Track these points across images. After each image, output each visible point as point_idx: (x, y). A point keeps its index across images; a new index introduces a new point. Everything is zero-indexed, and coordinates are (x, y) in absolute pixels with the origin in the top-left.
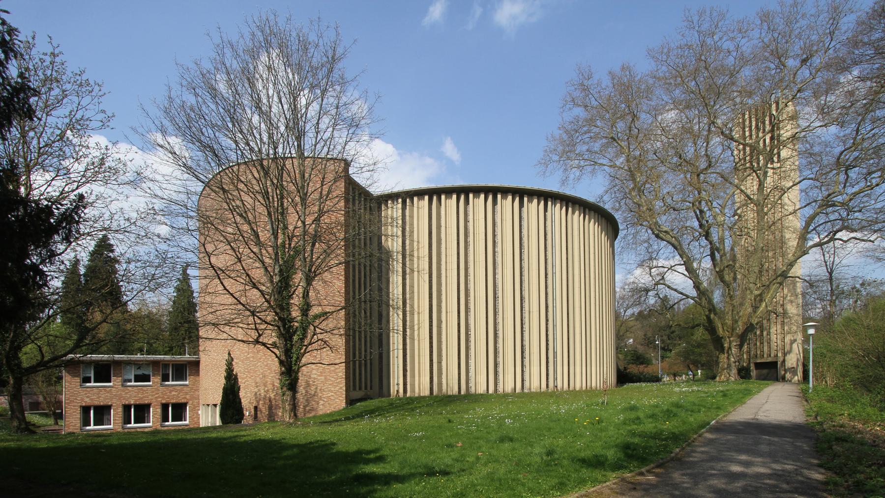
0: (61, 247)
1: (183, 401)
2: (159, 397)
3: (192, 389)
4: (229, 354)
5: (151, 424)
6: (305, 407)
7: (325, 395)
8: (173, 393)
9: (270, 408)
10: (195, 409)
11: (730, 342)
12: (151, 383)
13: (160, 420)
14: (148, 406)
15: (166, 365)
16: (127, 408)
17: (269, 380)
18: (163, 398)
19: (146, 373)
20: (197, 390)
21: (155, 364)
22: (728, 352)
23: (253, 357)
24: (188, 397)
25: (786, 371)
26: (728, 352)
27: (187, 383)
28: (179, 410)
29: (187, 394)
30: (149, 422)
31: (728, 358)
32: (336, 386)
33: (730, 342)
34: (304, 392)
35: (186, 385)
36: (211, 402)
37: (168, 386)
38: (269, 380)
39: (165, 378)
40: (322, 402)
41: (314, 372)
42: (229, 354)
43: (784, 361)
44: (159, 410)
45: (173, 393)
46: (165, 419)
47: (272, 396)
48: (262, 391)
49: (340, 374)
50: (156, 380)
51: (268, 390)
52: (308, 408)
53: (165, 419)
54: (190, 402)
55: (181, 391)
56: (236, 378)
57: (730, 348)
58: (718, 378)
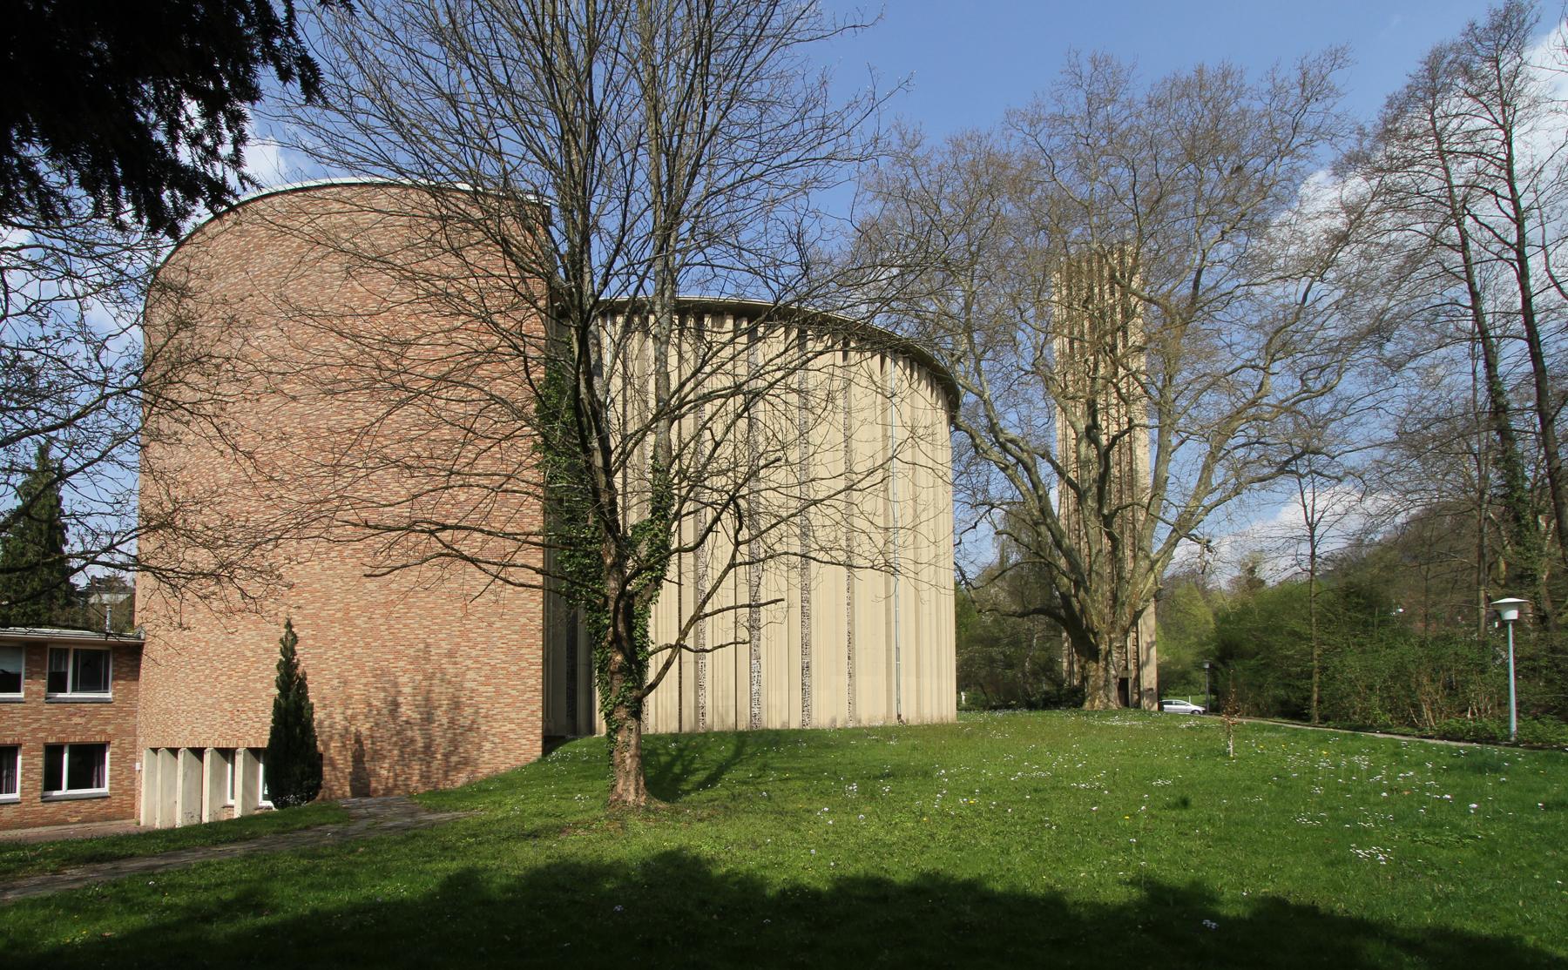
0: (1321, 176)
1: (99, 739)
2: (40, 729)
3: (120, 710)
4: (289, 625)
5: (17, 796)
6: (446, 756)
7: (497, 727)
8: (76, 720)
9: (358, 758)
10: (126, 760)
11: (1111, 641)
12: (21, 695)
13: (40, 785)
14: (101, 748)
15: (58, 651)
16: (53, 753)
17: (357, 691)
18: (51, 732)
19: (10, 669)
20: (132, 713)
21: (34, 649)
22: (1106, 659)
23: (314, 637)
24: (110, 729)
25: (1139, 693)
26: (1106, 659)
27: (109, 695)
28: (87, 763)
29: (107, 721)
30: (12, 790)
31: (1106, 670)
32: (521, 709)
33: (1111, 641)
34: (445, 721)
35: (18, 701)
36: (183, 741)
37: (65, 701)
38: (357, 691)
39: (57, 684)
40: (487, 746)
41: (471, 675)
42: (289, 625)
43: (1138, 678)
44: (40, 762)
45: (76, 720)
46: (52, 781)
47: (364, 729)
48: (338, 718)
49: (532, 682)
50: (32, 688)
51: (353, 717)
52: (454, 759)
53: (52, 781)
54: (116, 742)
55: (94, 715)
56: (302, 685)
57: (1109, 652)
58: (1087, 705)
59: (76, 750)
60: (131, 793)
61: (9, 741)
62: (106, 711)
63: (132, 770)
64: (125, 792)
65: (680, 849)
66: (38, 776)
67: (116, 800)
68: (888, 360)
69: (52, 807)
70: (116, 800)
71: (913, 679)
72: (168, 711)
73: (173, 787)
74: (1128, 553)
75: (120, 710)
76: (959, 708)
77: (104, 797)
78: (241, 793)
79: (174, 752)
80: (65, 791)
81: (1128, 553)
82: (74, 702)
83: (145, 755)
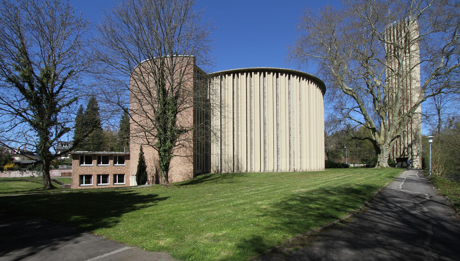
1: (123, 173)
10: (128, 177)
16: (99, 176)
24: (125, 171)
29: (124, 170)
55: (122, 168)
62: (124, 168)
66: (112, 180)
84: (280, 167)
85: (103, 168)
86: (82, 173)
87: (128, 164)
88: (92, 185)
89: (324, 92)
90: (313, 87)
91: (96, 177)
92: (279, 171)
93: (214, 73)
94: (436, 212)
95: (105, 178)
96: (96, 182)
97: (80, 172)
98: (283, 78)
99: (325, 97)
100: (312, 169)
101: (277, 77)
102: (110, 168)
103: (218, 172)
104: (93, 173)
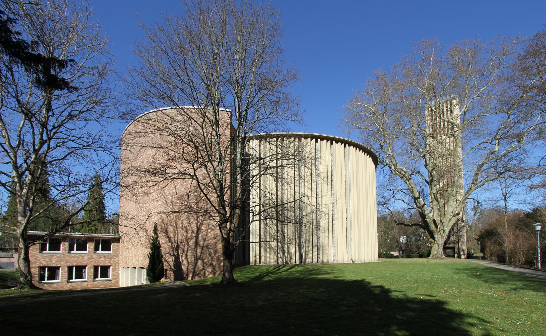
1: (108, 264)
2: (92, 261)
3: (114, 256)
8: (102, 259)
10: (116, 270)
13: (92, 277)
16: (70, 269)
20: (118, 257)
24: (111, 262)
28: (105, 271)
29: (111, 259)
36: (131, 265)
45: (102, 259)
53: (96, 276)
54: (113, 265)
55: (107, 258)
59: (102, 267)
60: (118, 280)
61: (84, 265)
62: (110, 256)
63: (118, 273)
64: (116, 279)
65: (363, 280)
66: (92, 274)
67: (113, 281)
68: (262, 142)
69: (96, 283)
70: (113, 281)
71: (357, 248)
72: (126, 257)
73: (128, 278)
74: (498, 276)
75: (114, 256)
76: (380, 256)
77: (110, 280)
78: (140, 279)
79: (135, 268)
80: (74, 280)
81: (498, 276)
82: (102, 254)
83: (121, 269)
84: (335, 258)
85: (77, 258)
86: (44, 263)
87: (117, 251)
88: (60, 281)
89: (376, 164)
90: (369, 160)
91: (66, 269)
92: (262, 255)
93: (294, 133)
94: (270, 272)
95: (80, 271)
96: (66, 277)
97: (40, 262)
98: (338, 147)
99: (378, 171)
100: (370, 259)
101: (332, 144)
102: (89, 257)
103: (255, 263)
104: (62, 263)
